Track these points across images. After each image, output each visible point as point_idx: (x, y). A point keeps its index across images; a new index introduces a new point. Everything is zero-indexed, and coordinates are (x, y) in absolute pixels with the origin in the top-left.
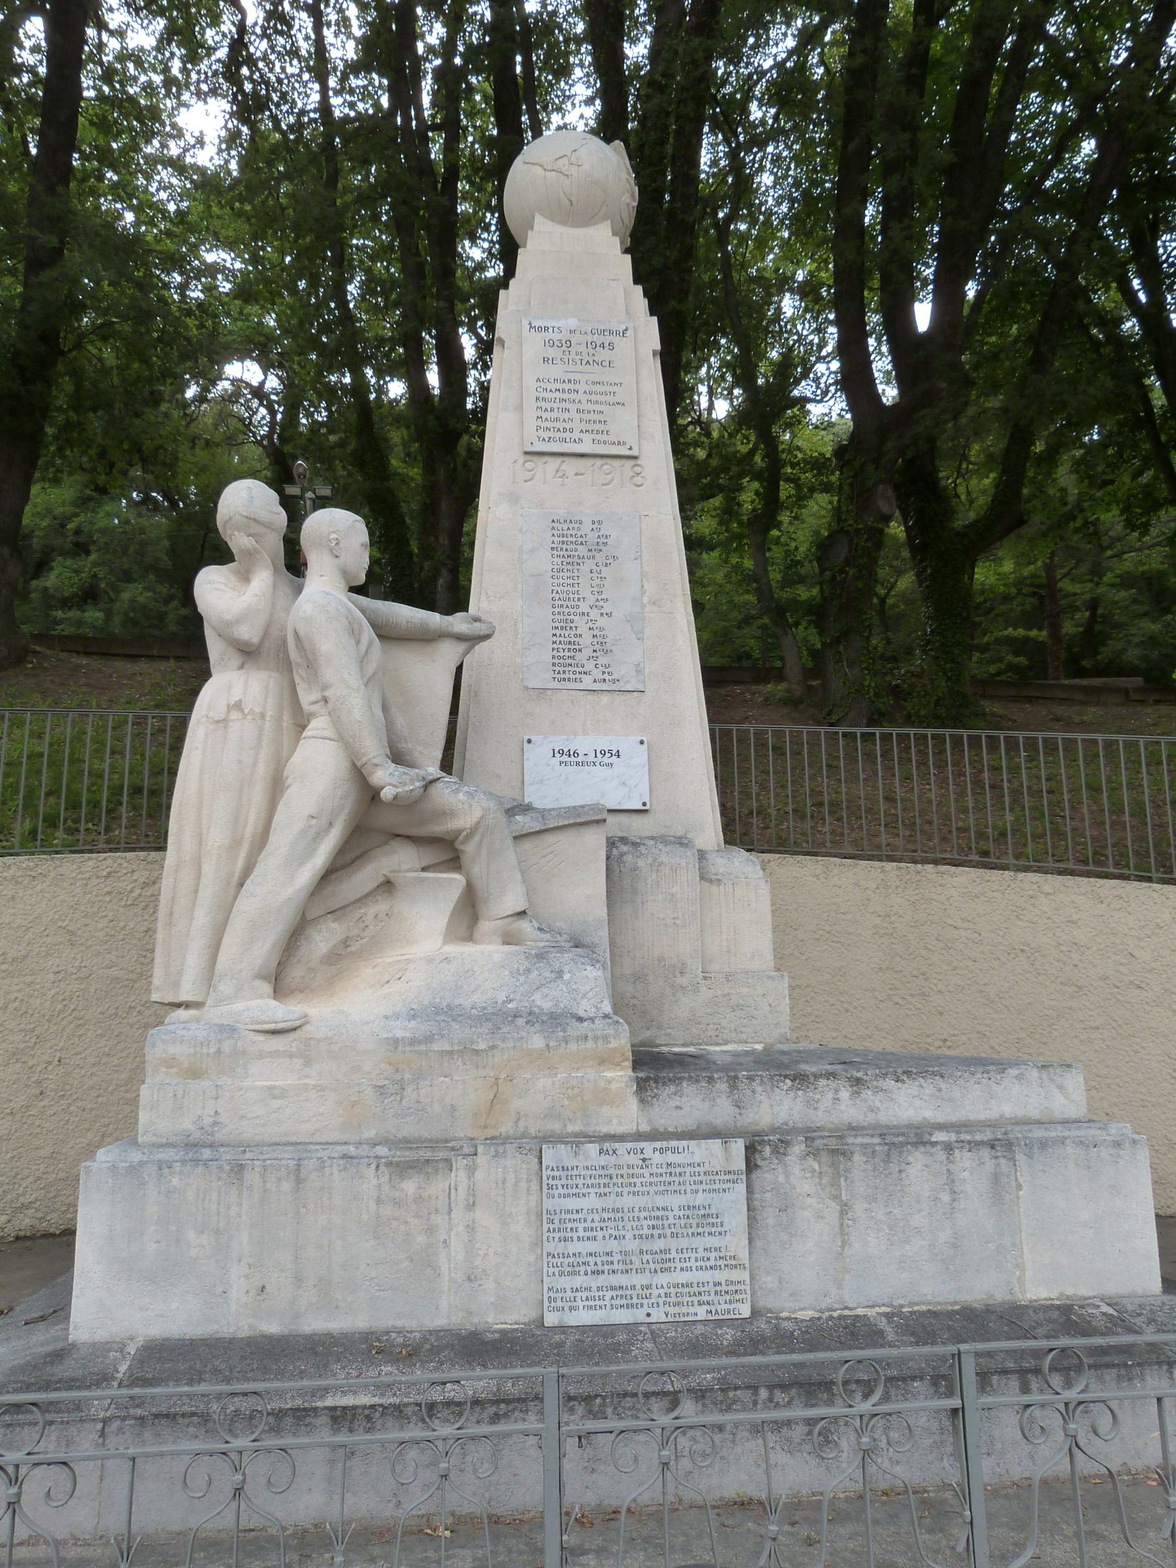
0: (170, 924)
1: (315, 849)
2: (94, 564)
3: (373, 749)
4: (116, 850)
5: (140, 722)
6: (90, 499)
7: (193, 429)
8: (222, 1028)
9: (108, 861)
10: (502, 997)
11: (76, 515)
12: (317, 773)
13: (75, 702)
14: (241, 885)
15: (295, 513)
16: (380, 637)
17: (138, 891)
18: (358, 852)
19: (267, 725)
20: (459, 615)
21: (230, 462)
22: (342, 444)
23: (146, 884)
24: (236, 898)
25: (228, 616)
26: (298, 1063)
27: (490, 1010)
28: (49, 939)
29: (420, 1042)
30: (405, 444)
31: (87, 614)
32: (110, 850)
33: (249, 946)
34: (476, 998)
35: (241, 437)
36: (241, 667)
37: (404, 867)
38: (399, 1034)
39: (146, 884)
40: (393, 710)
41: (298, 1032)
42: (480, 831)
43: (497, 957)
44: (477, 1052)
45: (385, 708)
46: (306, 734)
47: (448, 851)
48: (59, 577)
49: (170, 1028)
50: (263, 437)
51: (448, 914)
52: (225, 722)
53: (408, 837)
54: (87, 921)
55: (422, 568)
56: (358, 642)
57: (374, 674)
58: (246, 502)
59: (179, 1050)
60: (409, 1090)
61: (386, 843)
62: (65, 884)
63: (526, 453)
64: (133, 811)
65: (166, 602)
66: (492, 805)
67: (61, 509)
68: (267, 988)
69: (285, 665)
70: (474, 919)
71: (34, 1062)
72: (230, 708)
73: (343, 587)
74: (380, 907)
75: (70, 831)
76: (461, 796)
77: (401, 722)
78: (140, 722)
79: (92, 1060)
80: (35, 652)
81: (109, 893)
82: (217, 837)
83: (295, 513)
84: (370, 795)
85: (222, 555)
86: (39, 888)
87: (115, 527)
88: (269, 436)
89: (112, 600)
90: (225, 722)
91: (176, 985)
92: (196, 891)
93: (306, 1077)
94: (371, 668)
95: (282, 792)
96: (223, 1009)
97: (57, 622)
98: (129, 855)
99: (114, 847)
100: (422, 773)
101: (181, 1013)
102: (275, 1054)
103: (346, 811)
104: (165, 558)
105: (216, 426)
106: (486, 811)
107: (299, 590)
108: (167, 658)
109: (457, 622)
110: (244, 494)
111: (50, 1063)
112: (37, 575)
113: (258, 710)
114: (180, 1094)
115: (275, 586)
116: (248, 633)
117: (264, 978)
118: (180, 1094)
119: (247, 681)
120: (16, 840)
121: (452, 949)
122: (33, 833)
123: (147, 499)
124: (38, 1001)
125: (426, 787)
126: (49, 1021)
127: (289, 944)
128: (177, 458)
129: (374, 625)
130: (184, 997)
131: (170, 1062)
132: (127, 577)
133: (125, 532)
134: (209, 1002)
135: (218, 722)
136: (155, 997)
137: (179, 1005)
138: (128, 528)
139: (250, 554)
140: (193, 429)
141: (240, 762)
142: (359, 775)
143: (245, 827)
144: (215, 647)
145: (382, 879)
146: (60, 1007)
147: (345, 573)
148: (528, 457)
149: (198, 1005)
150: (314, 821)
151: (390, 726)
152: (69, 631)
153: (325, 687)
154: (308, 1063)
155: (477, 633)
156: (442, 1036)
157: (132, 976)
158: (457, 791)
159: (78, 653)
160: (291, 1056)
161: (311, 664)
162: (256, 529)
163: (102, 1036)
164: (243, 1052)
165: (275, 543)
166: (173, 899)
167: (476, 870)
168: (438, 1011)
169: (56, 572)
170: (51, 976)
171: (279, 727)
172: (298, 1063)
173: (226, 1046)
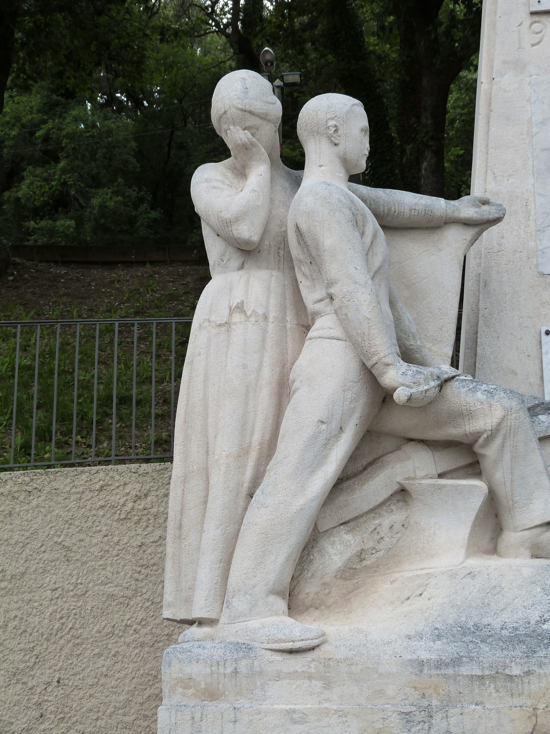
0: (179, 537)
1: (326, 457)
2: (64, 171)
3: (383, 348)
4: (108, 463)
5: (126, 329)
6: (57, 104)
7: (156, 21)
8: (238, 646)
9: (100, 474)
10: (534, 616)
11: (45, 122)
12: (325, 375)
13: (57, 312)
14: (251, 495)
15: (292, 101)
16: (384, 227)
17: (130, 505)
18: (370, 459)
19: (271, 327)
20: (465, 198)
21: (193, 54)
22: (312, 25)
23: (138, 498)
24: (245, 509)
25: (227, 215)
26: (317, 685)
27: (522, 631)
28: (46, 556)
29: (447, 665)
30: (379, 17)
31: (58, 223)
32: (100, 463)
33: (262, 560)
34: (505, 617)
35: (204, 27)
36: (242, 267)
37: (419, 474)
38: (424, 655)
39: (138, 498)
40: (400, 305)
41: (317, 651)
42: (502, 432)
43: (526, 572)
44: (511, 678)
45: (392, 304)
46: (310, 334)
47: (467, 456)
48: (30, 186)
49: (185, 646)
50: (226, 26)
51: (469, 525)
52: (227, 325)
53: (422, 442)
54: (82, 536)
55: (403, 151)
56: (363, 234)
57: (380, 267)
58: (241, 96)
59: (195, 670)
60: (438, 717)
61: (398, 448)
62: (60, 499)
63: (533, 13)
64: (133, 419)
65: (136, 206)
66: (514, 403)
67: (29, 117)
68: (281, 604)
69: (286, 262)
70: (498, 529)
71: (34, 682)
72: (231, 311)
73: (343, 176)
74: (394, 517)
75: (59, 445)
76: (479, 395)
77: (408, 317)
78: (126, 329)
79: (90, 681)
80: (15, 264)
81: (102, 507)
82: (224, 446)
83: (292, 101)
84: (382, 397)
85: (218, 151)
86: (35, 503)
87: (82, 132)
88: (233, 23)
89: (82, 207)
90: (227, 325)
91: (188, 601)
92: (206, 502)
93: (327, 700)
94: (377, 261)
95: (289, 396)
96: (238, 626)
97: (29, 233)
98: (121, 467)
99: (105, 461)
100: (436, 371)
101: (194, 631)
102: (293, 675)
103: (357, 414)
104: (133, 160)
105: (178, 17)
106: (508, 411)
107: (297, 183)
108: (143, 263)
109: (463, 208)
110: (239, 86)
111: (49, 684)
112: (8, 187)
113: (260, 311)
114: (198, 716)
115: (272, 180)
116: (248, 231)
117: (278, 593)
118: (198, 716)
119: (247, 282)
120: (10, 455)
121: (478, 563)
122: (26, 448)
123: (112, 100)
124: (37, 619)
125: (441, 386)
126: (47, 640)
127: (301, 557)
128: (143, 56)
129: (377, 215)
130: (196, 614)
131: (187, 683)
132: (96, 182)
133: (92, 136)
134: (223, 620)
135: (220, 325)
136: (167, 613)
137: (191, 623)
138: (95, 132)
139: (246, 148)
140: (156, 21)
141: (244, 366)
142: (370, 376)
143: (252, 433)
144: (213, 248)
145: (396, 487)
146: (57, 625)
147: (345, 161)
148: (536, 18)
149: (212, 622)
150: (324, 427)
151: (398, 321)
152: (42, 241)
153: (330, 284)
154: (328, 685)
155: (486, 217)
156: (471, 659)
157: (129, 593)
158: (474, 390)
159: (56, 263)
160: (310, 677)
161: (315, 260)
162: (252, 121)
163: (99, 655)
164: (261, 673)
165: (270, 133)
166: (182, 512)
167: (499, 476)
168: (464, 631)
169: (28, 181)
170: (49, 592)
171: (283, 329)
172: (317, 685)
173: (243, 666)
